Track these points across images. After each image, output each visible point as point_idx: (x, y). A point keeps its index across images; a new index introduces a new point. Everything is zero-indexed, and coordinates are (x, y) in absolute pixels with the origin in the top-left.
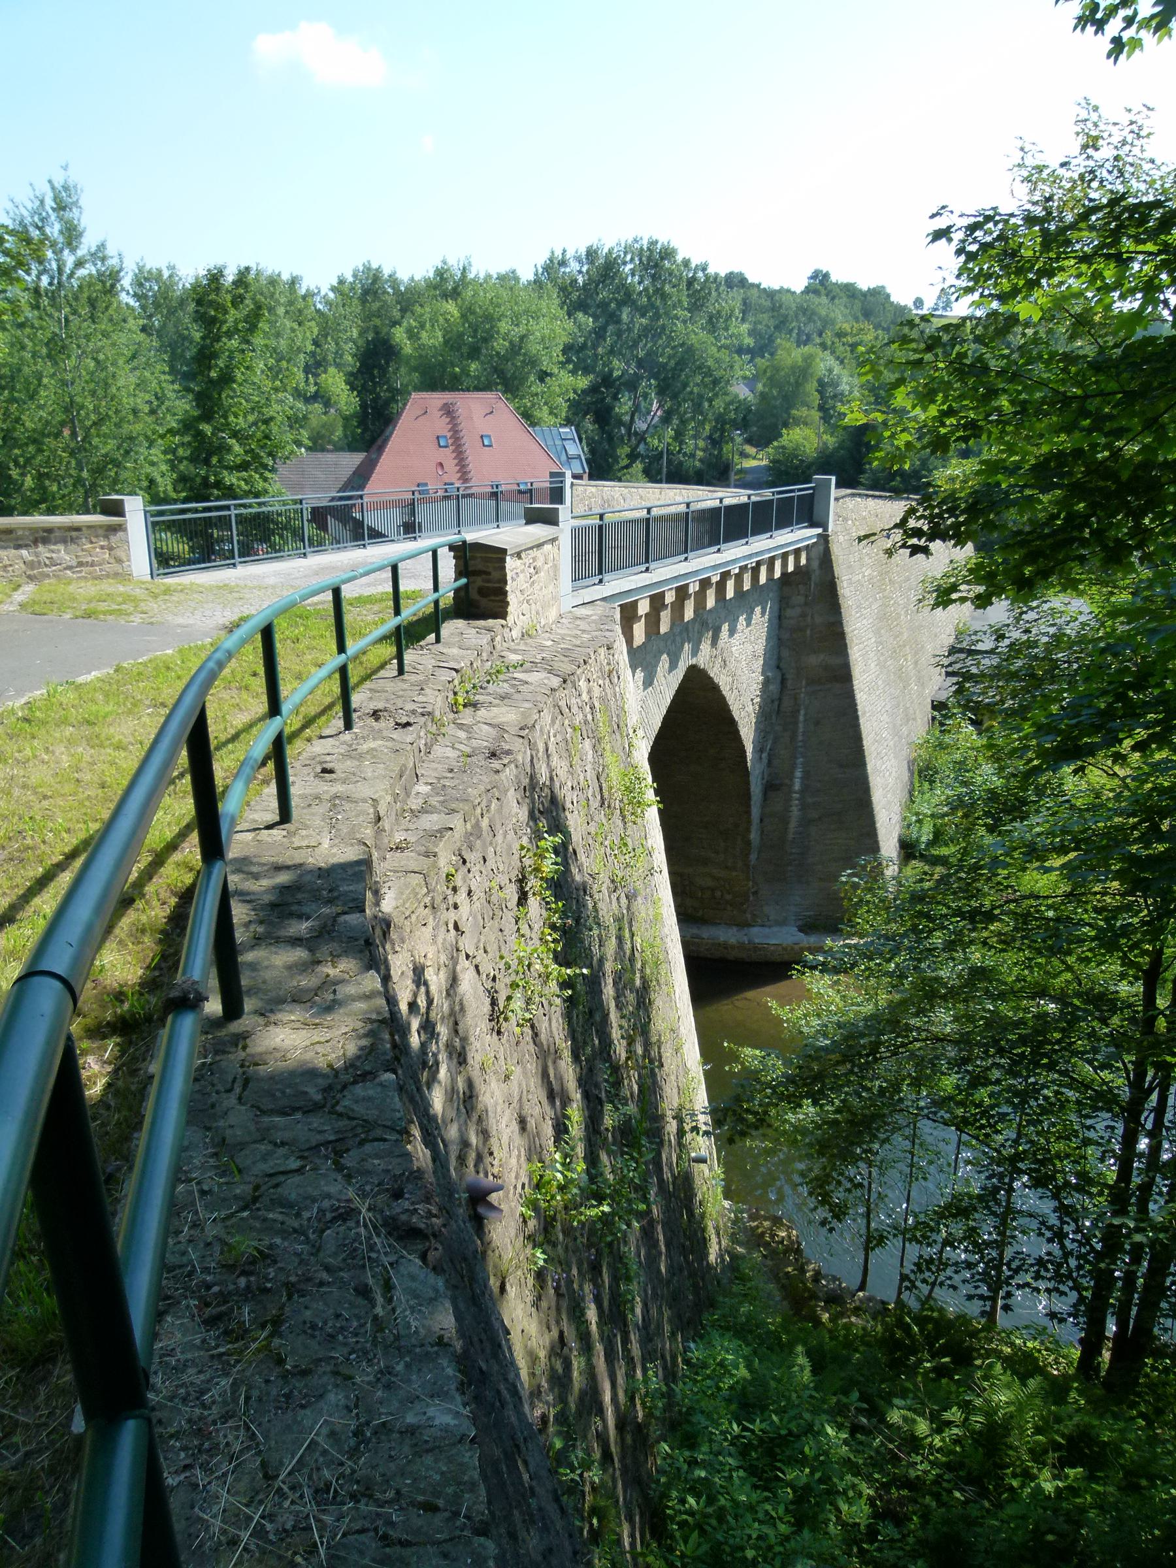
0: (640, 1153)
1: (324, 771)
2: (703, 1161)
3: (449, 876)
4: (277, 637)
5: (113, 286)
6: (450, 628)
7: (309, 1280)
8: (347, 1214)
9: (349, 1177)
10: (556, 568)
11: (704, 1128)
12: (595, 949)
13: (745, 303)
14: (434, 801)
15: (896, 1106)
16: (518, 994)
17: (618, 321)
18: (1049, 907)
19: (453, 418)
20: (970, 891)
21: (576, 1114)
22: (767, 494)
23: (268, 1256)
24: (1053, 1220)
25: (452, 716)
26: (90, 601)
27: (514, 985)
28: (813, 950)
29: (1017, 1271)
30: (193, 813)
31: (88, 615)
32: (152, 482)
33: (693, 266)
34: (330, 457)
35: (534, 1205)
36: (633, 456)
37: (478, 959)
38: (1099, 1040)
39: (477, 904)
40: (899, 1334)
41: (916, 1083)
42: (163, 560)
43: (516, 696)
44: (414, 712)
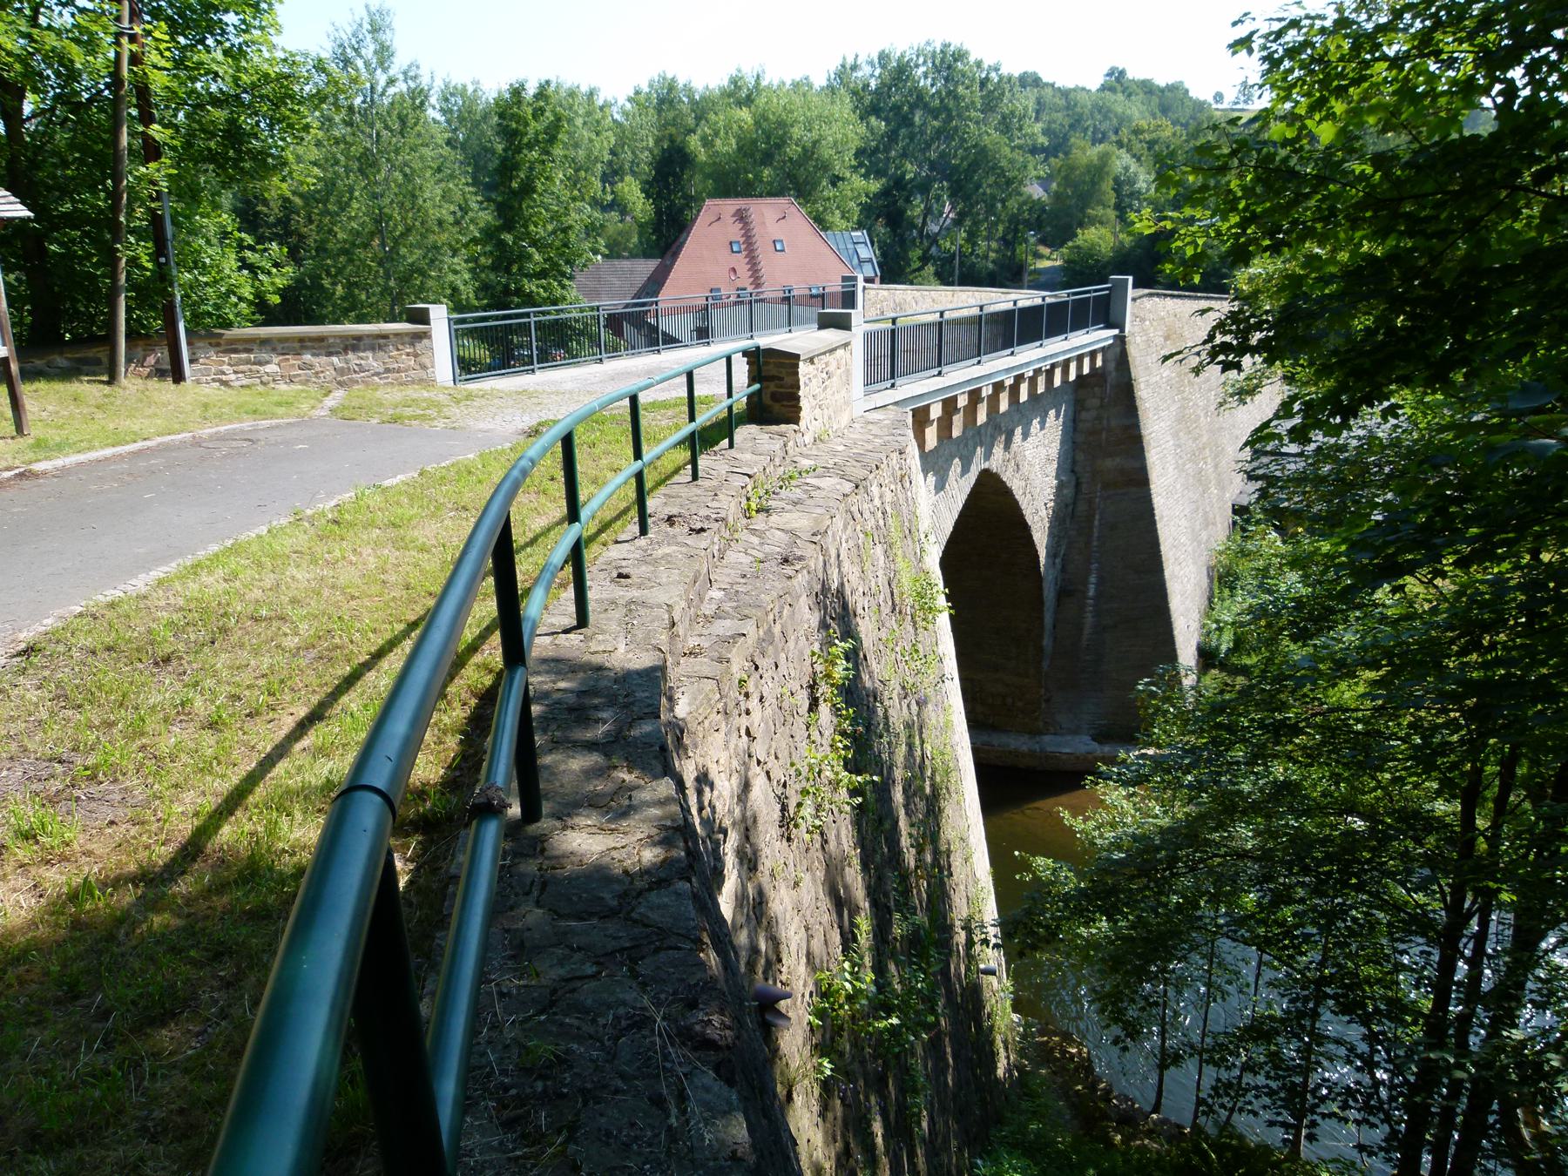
0: (928, 964)
1: (620, 576)
2: (992, 973)
3: (742, 682)
4: (576, 441)
5: (422, 103)
6: (743, 433)
7: (605, 1087)
8: (641, 1022)
9: (644, 985)
10: (848, 373)
11: (993, 941)
12: (885, 756)
13: (1039, 103)
14: (727, 606)
15: (1194, 923)
16: (808, 801)
17: (912, 124)
18: (1358, 721)
19: (746, 224)
20: (1272, 703)
21: (864, 924)
22: (1063, 295)
23: (565, 1061)
24: (1363, 1047)
25: (745, 521)
26: (396, 407)
27: (805, 792)
28: (1111, 761)
29: (1323, 1099)
30: (495, 614)
31: (395, 420)
32: (455, 290)
33: (985, 66)
34: (626, 264)
35: (820, 1014)
36: (925, 259)
37: (769, 765)
38: (1413, 860)
39: (769, 711)
40: (1195, 1161)
41: (1214, 900)
42: (466, 367)
43: (809, 502)
44: (708, 518)
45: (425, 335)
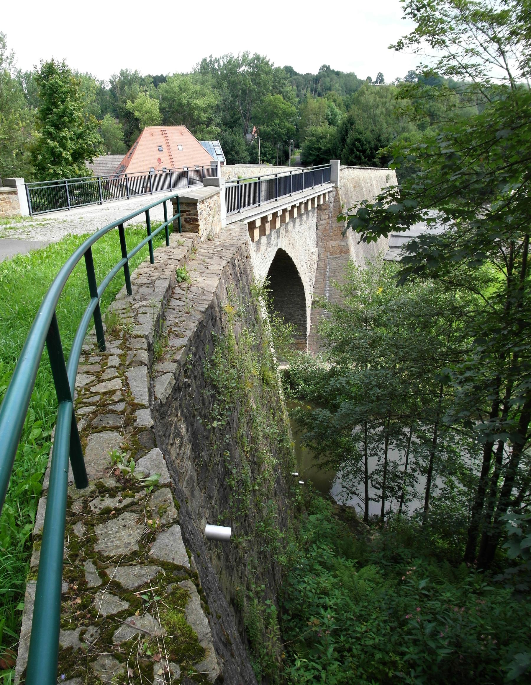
10: (219, 207)
42: (35, 208)
43: (208, 271)
45: (15, 193)
